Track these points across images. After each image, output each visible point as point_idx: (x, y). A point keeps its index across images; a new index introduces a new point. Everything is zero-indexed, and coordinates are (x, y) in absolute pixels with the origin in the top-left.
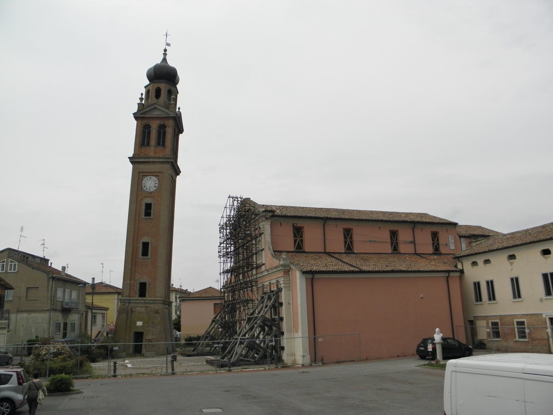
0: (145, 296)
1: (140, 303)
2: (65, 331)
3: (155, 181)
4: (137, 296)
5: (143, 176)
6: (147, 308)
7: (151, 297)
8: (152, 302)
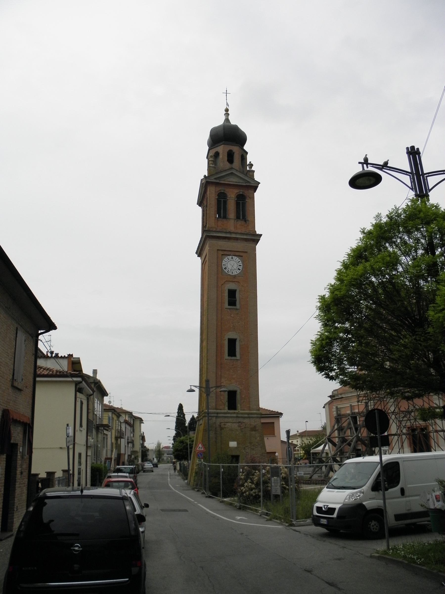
0: (235, 408)
1: (231, 417)
2: (191, 449)
3: (238, 262)
4: (227, 408)
5: (222, 255)
6: (240, 424)
7: (244, 410)
8: (246, 416)
